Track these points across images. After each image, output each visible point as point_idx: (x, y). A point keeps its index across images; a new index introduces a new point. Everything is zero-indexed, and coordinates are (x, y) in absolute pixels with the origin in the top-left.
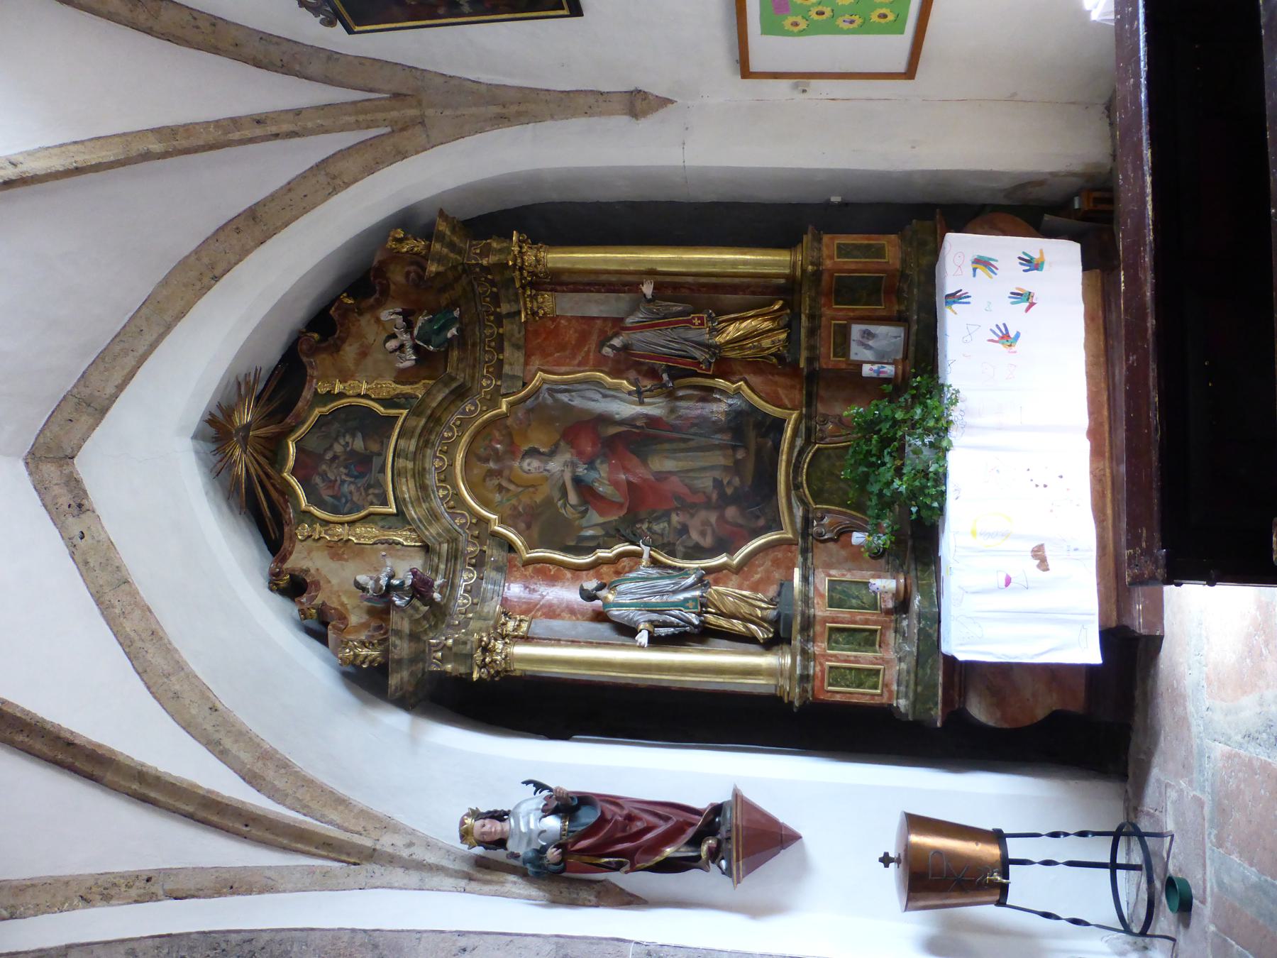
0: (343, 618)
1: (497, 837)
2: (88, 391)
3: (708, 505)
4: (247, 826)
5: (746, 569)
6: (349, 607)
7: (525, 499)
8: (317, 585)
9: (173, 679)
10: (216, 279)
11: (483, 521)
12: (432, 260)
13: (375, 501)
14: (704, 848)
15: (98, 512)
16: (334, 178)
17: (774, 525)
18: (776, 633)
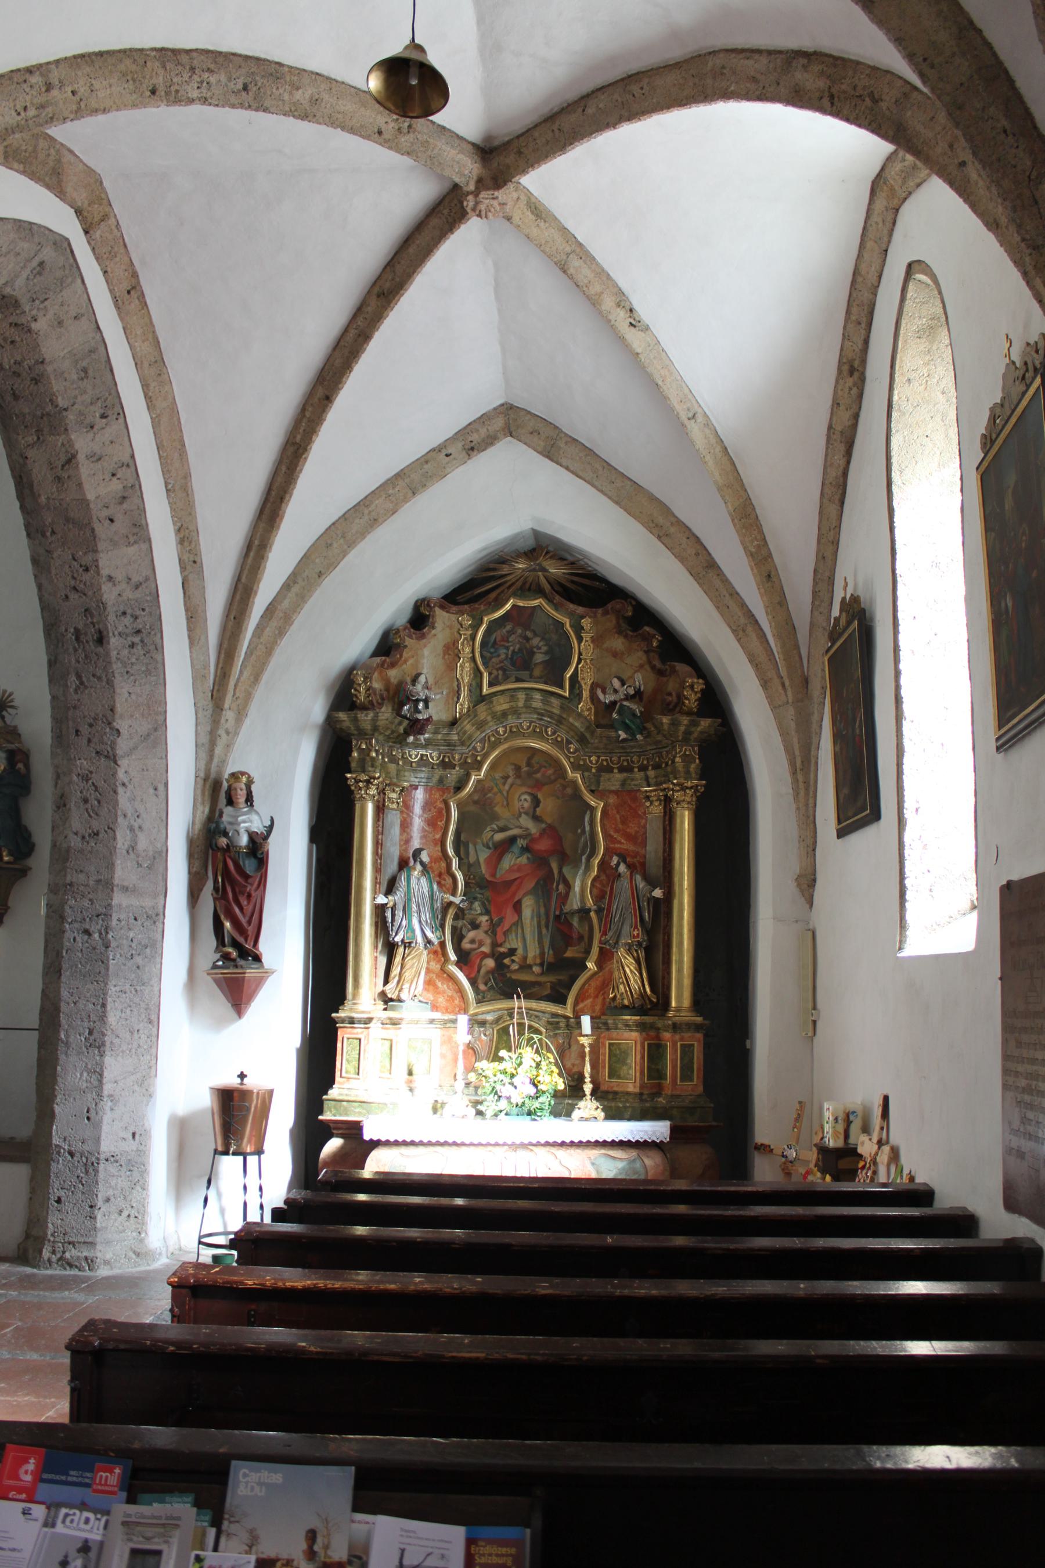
0: (393, 665)
1: (234, 800)
2: (562, 445)
3: (495, 945)
4: (234, 618)
5: (445, 975)
6: (405, 666)
7: (498, 798)
8: (423, 636)
9: (342, 541)
10: (659, 537)
11: (479, 765)
12: (672, 719)
13: (493, 676)
14: (230, 950)
15: (469, 462)
16: (744, 631)
17: (480, 997)
18: (392, 1000)
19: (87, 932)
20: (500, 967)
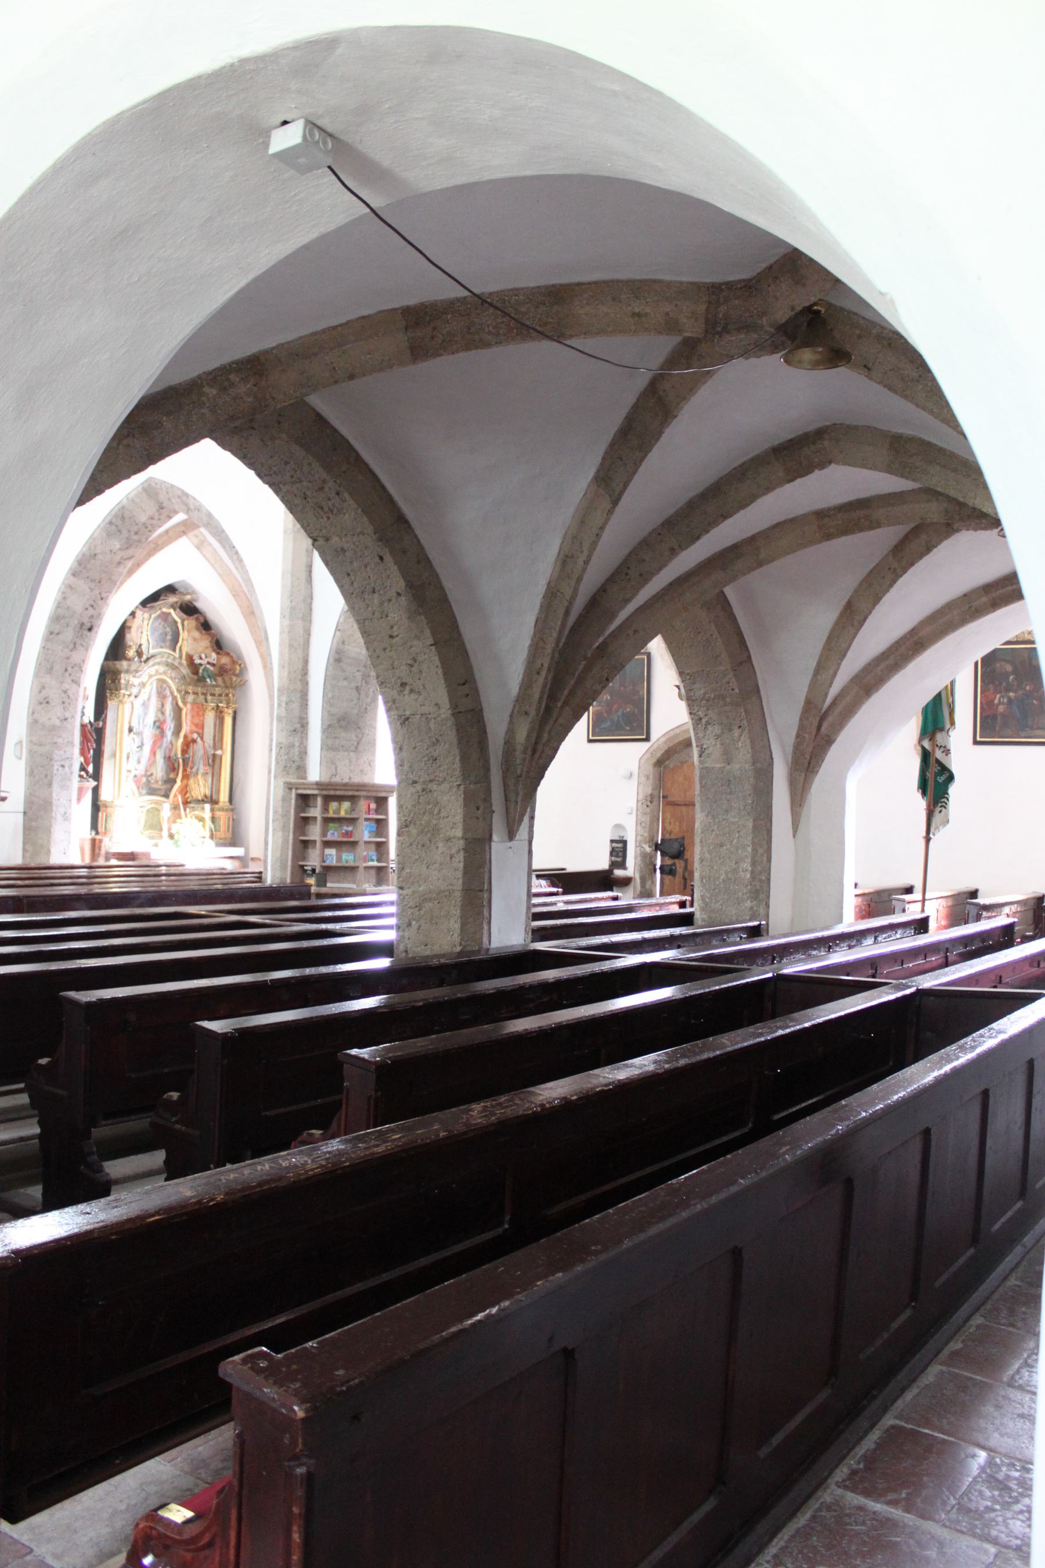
10: (234, 595)
19: (63, 766)
20: (148, 781)
